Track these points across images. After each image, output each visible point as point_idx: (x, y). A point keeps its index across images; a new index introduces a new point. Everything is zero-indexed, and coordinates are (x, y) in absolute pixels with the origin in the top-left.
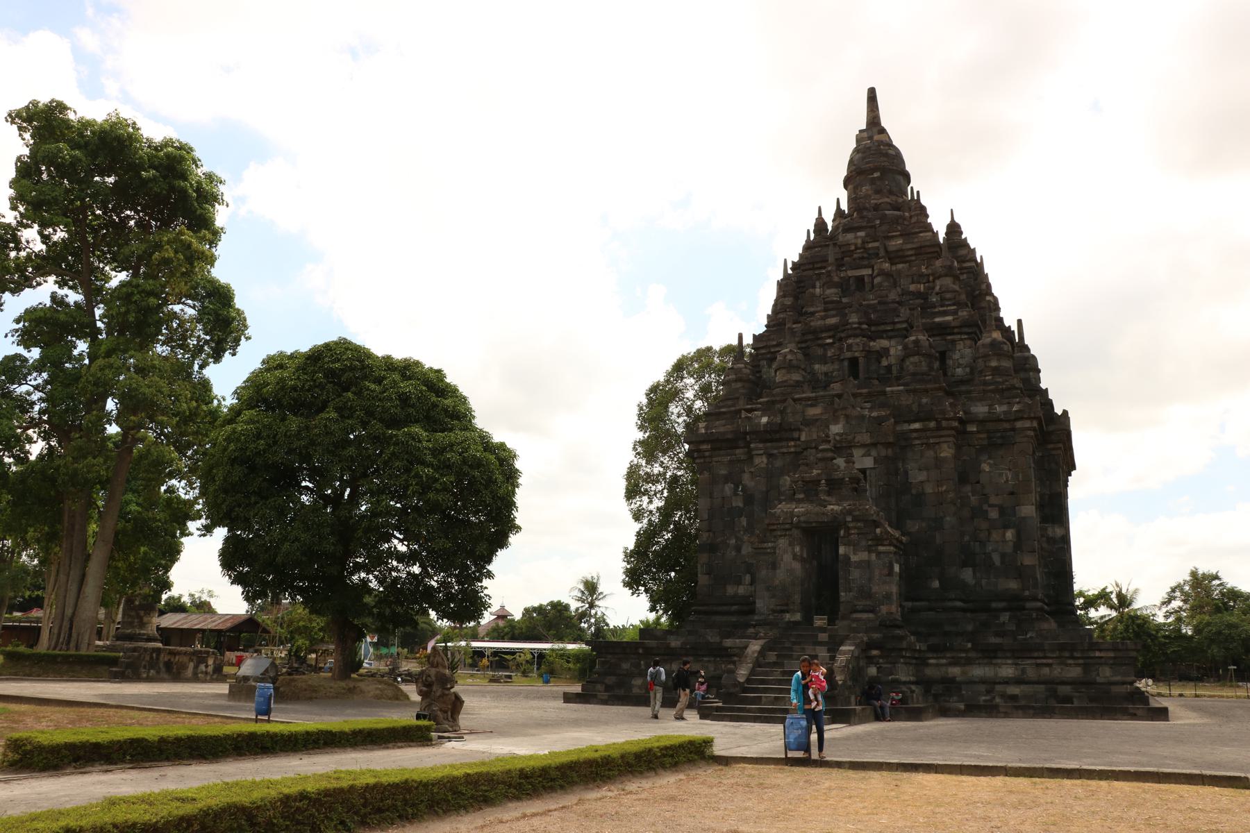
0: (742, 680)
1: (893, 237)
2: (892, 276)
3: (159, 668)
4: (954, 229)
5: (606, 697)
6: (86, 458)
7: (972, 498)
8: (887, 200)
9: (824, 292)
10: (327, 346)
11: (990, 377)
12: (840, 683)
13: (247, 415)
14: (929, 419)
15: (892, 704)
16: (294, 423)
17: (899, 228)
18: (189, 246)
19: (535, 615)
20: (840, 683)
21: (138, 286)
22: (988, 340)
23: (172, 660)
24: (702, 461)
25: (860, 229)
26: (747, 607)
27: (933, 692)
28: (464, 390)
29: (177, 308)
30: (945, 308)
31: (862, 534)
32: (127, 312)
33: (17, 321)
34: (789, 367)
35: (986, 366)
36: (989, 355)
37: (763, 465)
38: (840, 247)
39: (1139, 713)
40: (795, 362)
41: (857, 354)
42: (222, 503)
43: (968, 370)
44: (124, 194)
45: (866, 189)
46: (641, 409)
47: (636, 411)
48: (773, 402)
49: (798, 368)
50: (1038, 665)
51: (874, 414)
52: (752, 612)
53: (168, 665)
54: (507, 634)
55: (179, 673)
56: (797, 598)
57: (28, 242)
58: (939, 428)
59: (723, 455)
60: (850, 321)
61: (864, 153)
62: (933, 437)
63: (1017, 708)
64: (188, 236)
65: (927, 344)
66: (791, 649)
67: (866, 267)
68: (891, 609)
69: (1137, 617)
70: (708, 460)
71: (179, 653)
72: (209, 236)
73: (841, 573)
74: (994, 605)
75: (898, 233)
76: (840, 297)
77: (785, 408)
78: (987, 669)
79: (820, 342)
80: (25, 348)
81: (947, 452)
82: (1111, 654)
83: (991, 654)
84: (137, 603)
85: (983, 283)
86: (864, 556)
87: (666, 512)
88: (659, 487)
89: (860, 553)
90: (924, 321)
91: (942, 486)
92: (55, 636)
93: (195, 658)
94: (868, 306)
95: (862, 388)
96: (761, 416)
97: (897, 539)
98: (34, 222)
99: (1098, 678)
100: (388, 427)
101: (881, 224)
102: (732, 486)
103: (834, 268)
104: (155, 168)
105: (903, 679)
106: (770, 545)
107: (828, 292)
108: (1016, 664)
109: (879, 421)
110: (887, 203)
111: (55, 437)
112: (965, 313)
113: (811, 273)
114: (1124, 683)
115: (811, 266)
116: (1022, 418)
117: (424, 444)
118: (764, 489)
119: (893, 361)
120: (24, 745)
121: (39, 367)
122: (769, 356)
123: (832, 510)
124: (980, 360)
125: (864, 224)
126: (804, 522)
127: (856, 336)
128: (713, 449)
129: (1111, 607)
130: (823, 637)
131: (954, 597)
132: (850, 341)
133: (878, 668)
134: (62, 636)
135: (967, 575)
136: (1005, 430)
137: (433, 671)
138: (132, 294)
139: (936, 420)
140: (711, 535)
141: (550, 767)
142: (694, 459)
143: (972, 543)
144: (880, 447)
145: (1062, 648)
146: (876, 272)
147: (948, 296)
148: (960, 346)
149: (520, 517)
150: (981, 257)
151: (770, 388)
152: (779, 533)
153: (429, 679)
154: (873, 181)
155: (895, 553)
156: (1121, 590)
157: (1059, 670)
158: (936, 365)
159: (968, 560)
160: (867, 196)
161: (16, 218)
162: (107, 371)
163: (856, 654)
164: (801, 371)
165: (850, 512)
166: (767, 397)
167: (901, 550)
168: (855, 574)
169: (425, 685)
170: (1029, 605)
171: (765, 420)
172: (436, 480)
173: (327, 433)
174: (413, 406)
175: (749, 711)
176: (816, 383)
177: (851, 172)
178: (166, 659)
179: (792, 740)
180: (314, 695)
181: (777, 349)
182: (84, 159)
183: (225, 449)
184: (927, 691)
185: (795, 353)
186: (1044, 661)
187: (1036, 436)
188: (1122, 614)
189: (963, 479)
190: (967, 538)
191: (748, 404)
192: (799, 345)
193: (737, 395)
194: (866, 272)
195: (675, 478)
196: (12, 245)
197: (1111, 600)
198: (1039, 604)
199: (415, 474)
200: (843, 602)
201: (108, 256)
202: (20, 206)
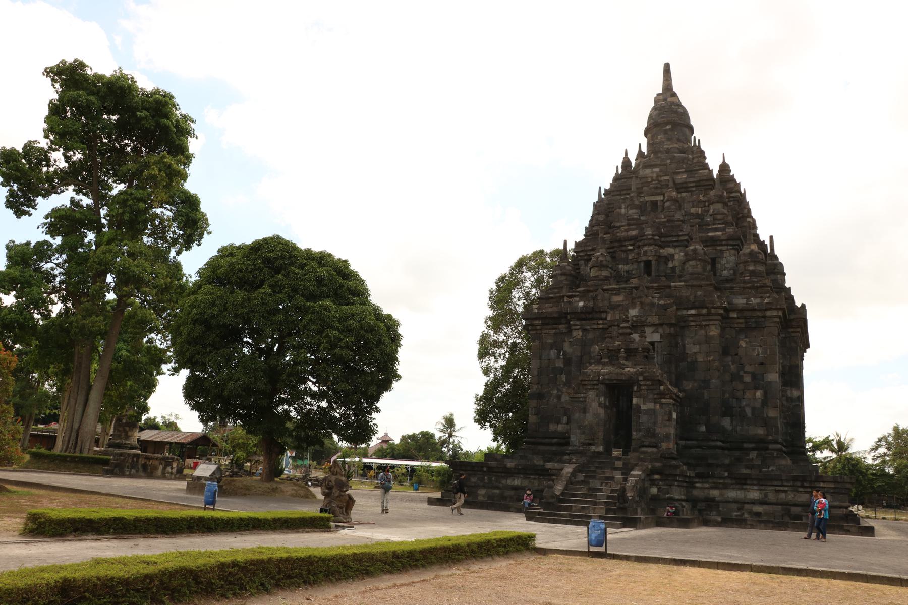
0: (558, 493)
1: (679, 173)
6: (91, 316)
9: (627, 212)
10: (265, 240)
11: (748, 278)
12: (630, 498)
13: (203, 290)
14: (702, 307)
15: (667, 515)
17: (684, 166)
18: (170, 166)
19: (409, 441)
20: (630, 498)
21: (131, 194)
22: (748, 251)
23: (148, 463)
24: (535, 332)
26: (564, 440)
27: (698, 507)
28: (363, 275)
29: (159, 211)
30: (716, 226)
31: (649, 389)
32: (124, 213)
33: (46, 217)
34: (601, 266)
36: (748, 262)
37: (579, 337)
38: (641, 179)
39: (853, 530)
40: (604, 263)
41: (650, 258)
43: (732, 272)
44: (123, 128)
46: (492, 293)
47: (488, 295)
48: (588, 291)
49: (607, 267)
50: (777, 491)
51: (662, 302)
53: (145, 467)
54: (389, 454)
55: (152, 473)
56: (601, 435)
57: (55, 161)
58: (709, 314)
59: (550, 329)
60: (646, 233)
61: (660, 110)
62: (704, 321)
63: (761, 522)
64: (169, 160)
65: (702, 251)
66: (594, 472)
68: (670, 446)
69: (852, 459)
70: (539, 332)
71: (152, 458)
72: (183, 160)
73: (634, 418)
74: (745, 445)
75: (684, 170)
76: (639, 216)
77: (596, 296)
78: (739, 492)
79: (624, 248)
81: (714, 331)
82: (832, 485)
83: (742, 482)
84: (124, 421)
86: (651, 406)
87: (507, 370)
88: (503, 351)
90: (700, 235)
91: (710, 356)
92: (66, 443)
93: (163, 462)
97: (675, 394)
98: (60, 147)
101: (671, 163)
102: (556, 351)
103: (636, 195)
104: (147, 110)
105: (677, 497)
106: (582, 395)
107: (631, 212)
109: (665, 307)
110: (675, 147)
111: (70, 300)
112: (731, 230)
113: (618, 197)
114: (841, 507)
115: (619, 193)
116: (770, 309)
117: (333, 313)
118: (579, 354)
119: (677, 264)
120: (40, 518)
121: (60, 250)
122: (585, 257)
123: (629, 371)
124: (741, 265)
125: (659, 163)
126: (608, 380)
127: (650, 245)
128: (543, 324)
129: (833, 451)
130: (619, 464)
132: (646, 248)
133: (658, 488)
134: (71, 442)
135: (726, 422)
136: (758, 317)
137: (333, 478)
138: (127, 200)
139: (707, 308)
140: (539, 386)
141: (415, 551)
142: (528, 331)
144: (665, 326)
145: (795, 479)
146: (666, 198)
147: (719, 217)
148: (726, 254)
149: (401, 369)
150: (744, 189)
151: (585, 281)
152: (589, 387)
153: (330, 484)
154: (666, 132)
155: (674, 405)
156: (840, 438)
157: (793, 495)
158: (709, 267)
159: (728, 411)
160: (661, 143)
161: (47, 144)
162: (108, 255)
163: (643, 477)
164: (608, 269)
165: (641, 374)
167: (678, 402)
168: (644, 419)
169: (328, 488)
170: (771, 446)
171: (581, 304)
172: (341, 340)
175: (562, 516)
176: (620, 278)
177: (650, 124)
179: (593, 538)
180: (247, 492)
181: (592, 253)
182: (96, 102)
183: (189, 313)
184: (694, 507)
185: (605, 256)
186: (781, 488)
187: (781, 322)
188: (840, 456)
189: (725, 352)
190: (727, 396)
191: (569, 292)
193: (561, 285)
194: (660, 198)
195: (515, 345)
196: (44, 163)
197: (833, 445)
198: (779, 446)
199: (326, 335)
201: (111, 172)
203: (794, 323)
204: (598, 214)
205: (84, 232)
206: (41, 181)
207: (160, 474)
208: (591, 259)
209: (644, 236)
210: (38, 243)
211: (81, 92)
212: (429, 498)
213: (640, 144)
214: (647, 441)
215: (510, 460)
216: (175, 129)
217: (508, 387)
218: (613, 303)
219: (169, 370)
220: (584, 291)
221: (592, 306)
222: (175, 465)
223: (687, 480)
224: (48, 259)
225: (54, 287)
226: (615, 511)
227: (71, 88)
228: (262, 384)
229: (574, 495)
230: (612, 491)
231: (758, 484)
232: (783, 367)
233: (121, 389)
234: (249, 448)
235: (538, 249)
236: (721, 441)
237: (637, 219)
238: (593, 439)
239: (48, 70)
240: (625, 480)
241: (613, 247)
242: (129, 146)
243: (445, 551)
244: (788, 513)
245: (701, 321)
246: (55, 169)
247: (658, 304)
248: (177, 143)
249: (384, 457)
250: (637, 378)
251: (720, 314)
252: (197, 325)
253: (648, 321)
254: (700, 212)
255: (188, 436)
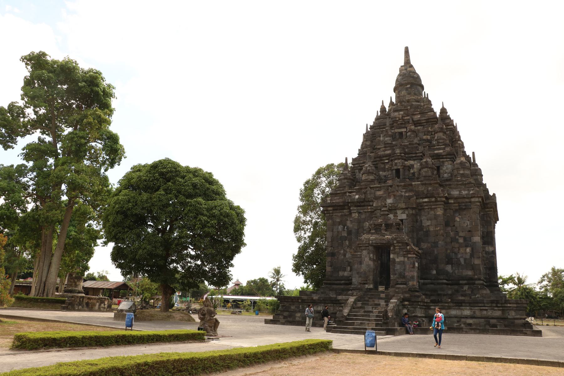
0: (345, 314)
1: (416, 114)
2: (415, 132)
3: (83, 305)
4: (443, 111)
5: (284, 322)
6: (52, 211)
7: (451, 233)
8: (413, 97)
10: (160, 161)
11: (460, 178)
12: (390, 316)
14: (432, 197)
15: (414, 327)
16: (145, 196)
17: (419, 110)
18: (100, 117)
19: (252, 284)
20: (390, 316)
21: (76, 134)
22: (459, 161)
24: (328, 215)
25: (401, 110)
26: (348, 282)
28: (221, 182)
32: (72, 145)
33: (23, 149)
34: (369, 173)
35: (458, 173)
36: (459, 168)
37: (356, 217)
38: (392, 118)
39: (528, 333)
40: (371, 171)
41: (399, 167)
42: (112, 232)
43: (450, 175)
45: (404, 93)
46: (301, 191)
47: (299, 192)
48: (361, 189)
49: (372, 173)
50: (481, 310)
51: (407, 194)
52: (351, 284)
53: (87, 304)
54: (239, 292)
55: (92, 308)
56: (371, 278)
57: (28, 114)
58: (436, 201)
60: (396, 152)
62: (434, 205)
63: (472, 329)
65: (431, 163)
67: (403, 128)
68: (414, 283)
69: (527, 289)
70: (331, 214)
71: (92, 299)
72: (108, 112)
73: (391, 266)
74: (461, 282)
75: (418, 113)
77: (366, 191)
78: (458, 311)
79: (382, 162)
80: (26, 161)
81: (440, 212)
82: (515, 305)
84: (74, 276)
85: (457, 135)
86: (402, 259)
87: (312, 238)
88: (309, 227)
89: (400, 258)
90: (430, 152)
91: (437, 227)
93: (99, 301)
94: (405, 145)
95: (401, 183)
96: (356, 195)
97: (417, 251)
99: (509, 316)
100: (187, 198)
101: (411, 108)
102: (342, 226)
103: (389, 128)
104: (85, 82)
105: (419, 315)
106: (359, 253)
107: (386, 139)
108: (471, 309)
109: (409, 198)
110: (413, 99)
111: (39, 201)
112: (449, 149)
114: (521, 319)
115: (379, 127)
116: (474, 197)
117: (203, 206)
121: (32, 170)
123: (388, 238)
124: (455, 170)
126: (375, 243)
127: (399, 159)
128: (333, 210)
129: (515, 284)
130: (383, 295)
131: (442, 278)
132: (396, 161)
133: (408, 310)
134: (41, 290)
135: (449, 268)
136: (467, 202)
137: (206, 309)
138: (74, 137)
139: (435, 197)
141: (258, 353)
142: (325, 214)
143: (451, 254)
146: (408, 130)
147: (441, 141)
148: (446, 164)
149: (246, 239)
150: (456, 123)
151: (359, 182)
152: (363, 248)
153: (204, 312)
154: (407, 89)
155: (416, 258)
156: (519, 276)
157: (491, 312)
158: (435, 172)
159: (449, 261)
160: (404, 96)
162: (62, 172)
163: (398, 303)
164: (373, 175)
165: (395, 239)
166: (358, 186)
167: (418, 256)
168: (398, 267)
169: (202, 315)
170: (477, 282)
171: (357, 197)
172: (208, 222)
173: (160, 201)
174: (198, 189)
176: (380, 180)
177: (397, 85)
178: (86, 301)
179: (368, 342)
181: (363, 165)
182: (54, 77)
183: (114, 207)
185: (371, 167)
186: (484, 308)
187: (481, 205)
188: (520, 287)
189: (447, 224)
190: (449, 251)
191: (349, 190)
192: (373, 163)
193: (344, 185)
195: (316, 223)
196: (21, 116)
197: (515, 280)
198: (482, 282)
199: (199, 219)
200: (392, 280)
201: (63, 121)
202: (25, 98)
203: (489, 206)
204: (366, 141)
205: (47, 158)
206: (19, 127)
207: (97, 309)
208: (362, 169)
209: (395, 153)
210: (18, 166)
211: (44, 71)
212: (265, 320)
213: (391, 97)
214: (400, 281)
215: (315, 295)
216: (102, 93)
217: (313, 249)
218: (377, 196)
219: (101, 243)
220: (358, 189)
221: (364, 198)
222: (106, 303)
223: (425, 305)
224: (25, 175)
225: (29, 193)
226: (381, 325)
227: (37, 69)
228: (160, 252)
229: (355, 316)
230: (379, 312)
231: (470, 306)
232: (483, 233)
233: (72, 256)
234: (152, 291)
235: (330, 163)
236: (447, 280)
237: (390, 144)
238: (366, 281)
239: (23, 58)
240: (387, 305)
241: (376, 161)
242: (74, 104)
243: (277, 353)
244: (488, 323)
245: (431, 205)
246: (28, 119)
247: (405, 195)
248: (104, 102)
249: (237, 294)
250: (393, 242)
251: (442, 201)
252: (119, 215)
253: (399, 206)
254: (429, 138)
255: (114, 284)
